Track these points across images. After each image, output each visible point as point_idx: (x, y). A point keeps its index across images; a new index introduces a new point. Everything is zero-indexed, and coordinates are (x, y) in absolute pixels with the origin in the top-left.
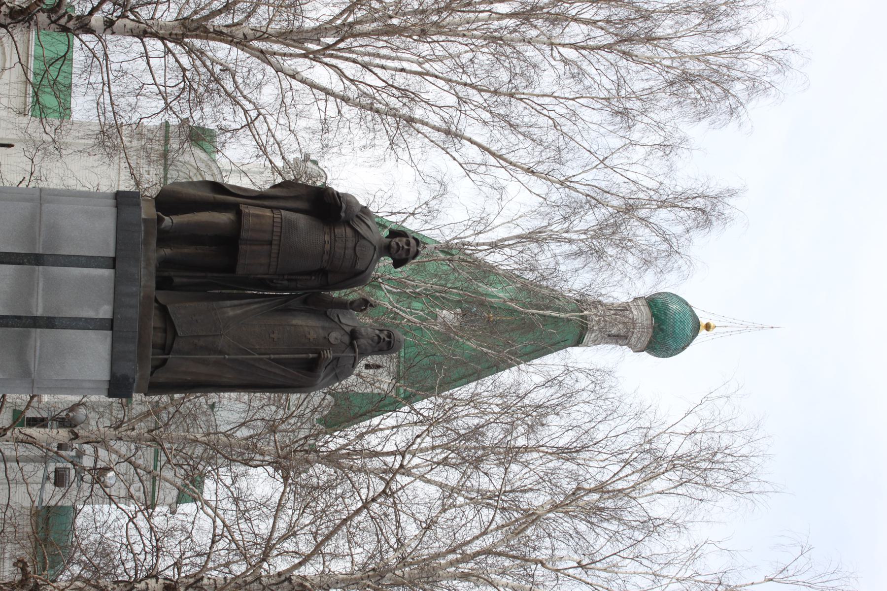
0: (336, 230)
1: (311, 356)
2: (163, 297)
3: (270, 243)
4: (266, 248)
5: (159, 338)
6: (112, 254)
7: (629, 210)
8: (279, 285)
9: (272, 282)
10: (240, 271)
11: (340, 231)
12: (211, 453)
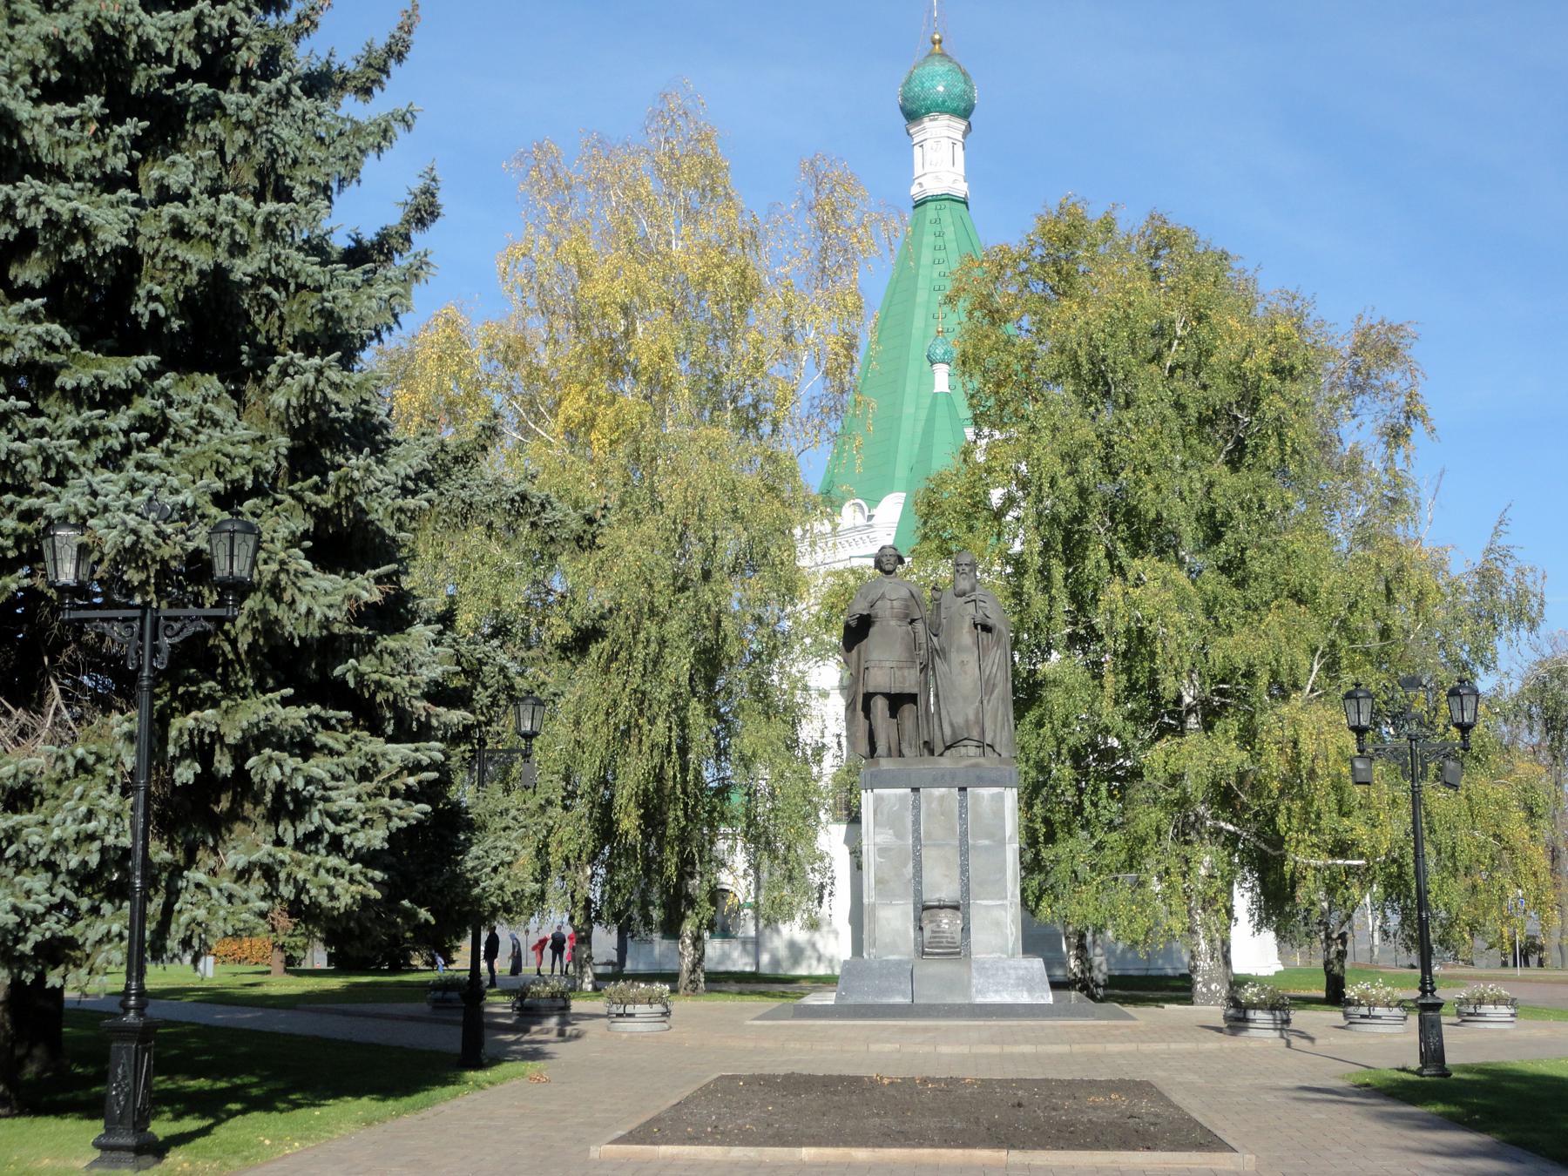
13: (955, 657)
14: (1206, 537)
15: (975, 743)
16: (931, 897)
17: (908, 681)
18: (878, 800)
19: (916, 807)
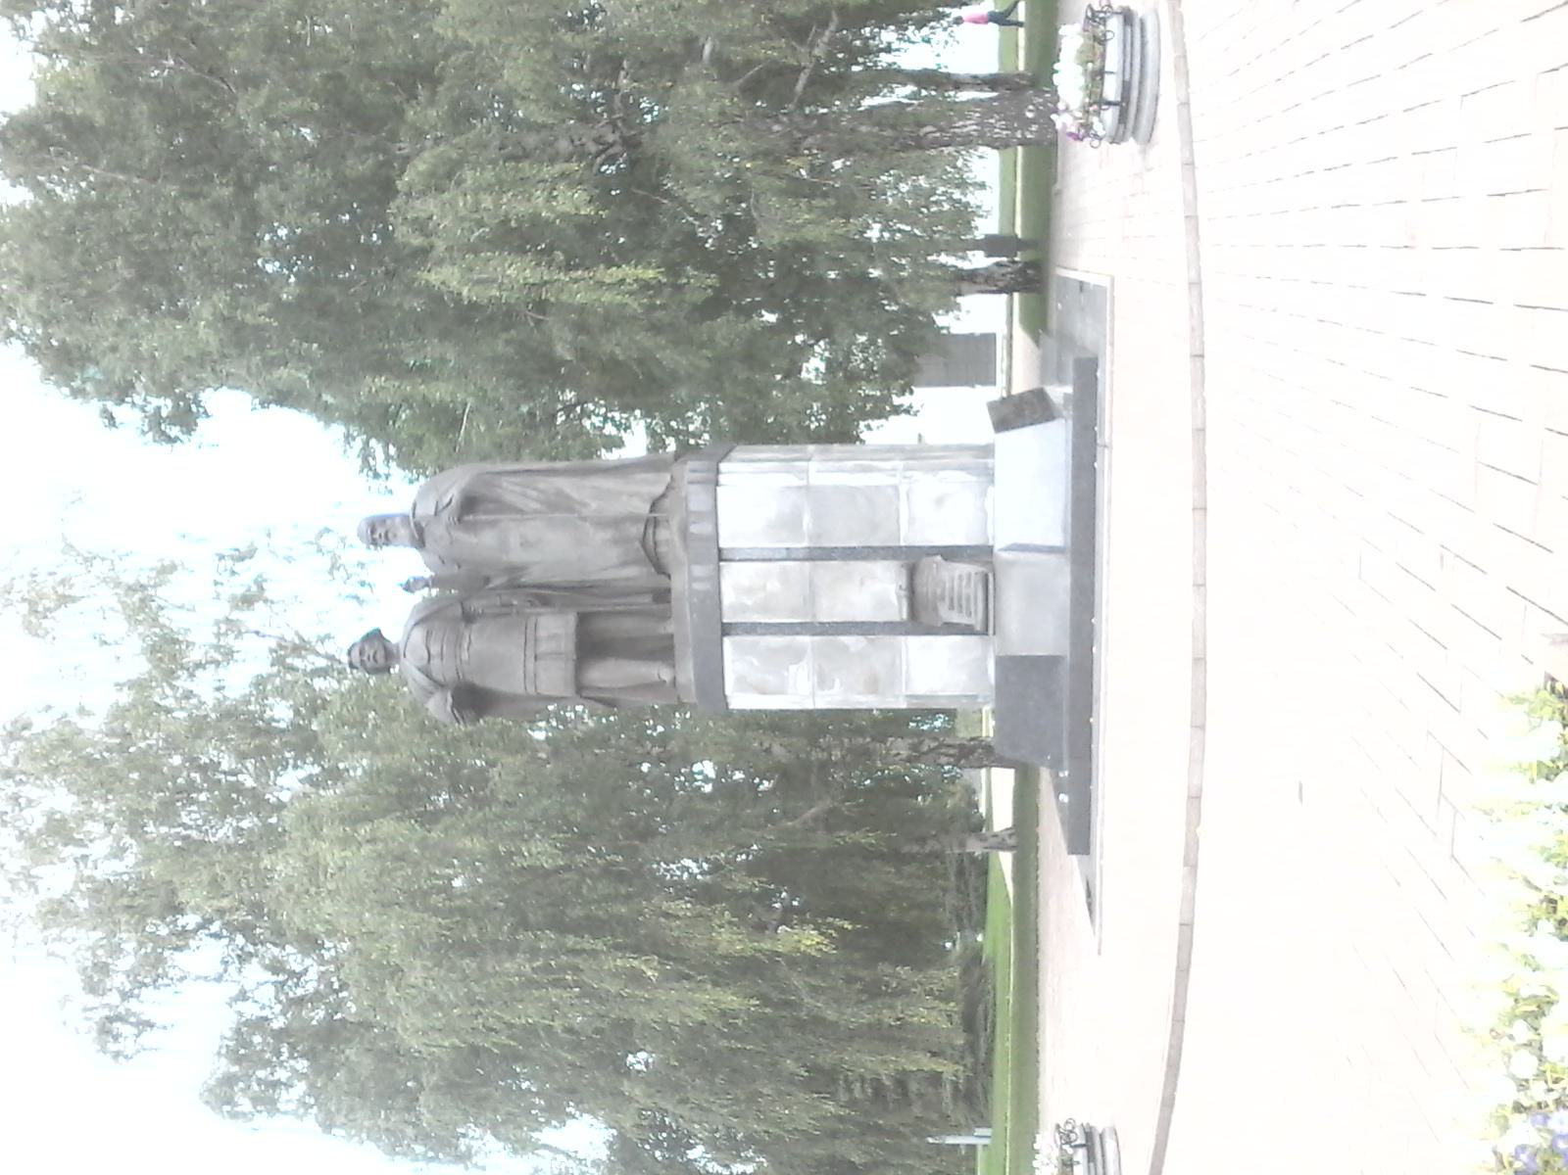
2: (662, 580)
5: (663, 534)
10: (571, 619)
13: (517, 556)
14: (280, 386)
15: (650, 531)
16: (898, 611)
17: (556, 629)
18: (744, 684)
19: (752, 629)
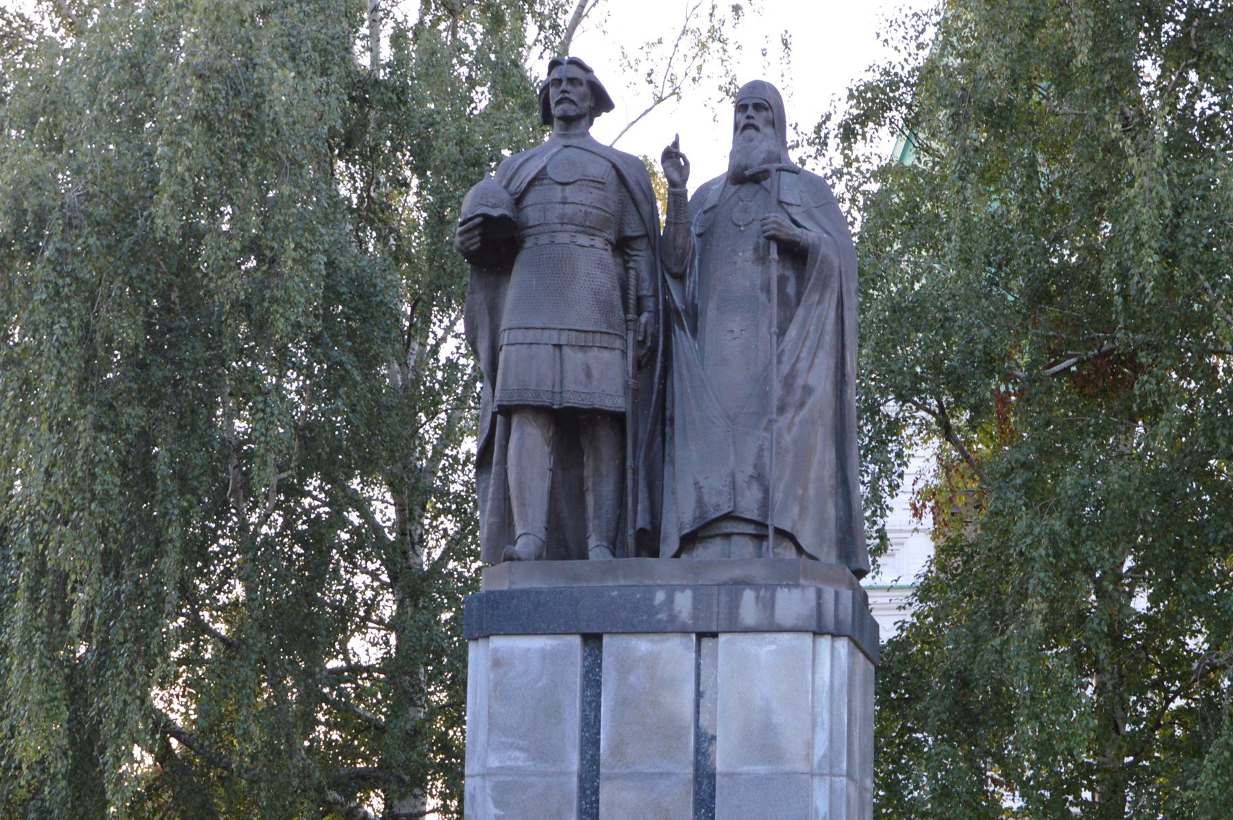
0: (531, 223)
1: (774, 254)
2: (670, 543)
3: (559, 346)
4: (567, 351)
6: (577, 640)
7: (1061, 208)
8: (650, 331)
9: (644, 342)
11: (532, 214)
12: (179, 169)
15: (750, 529)
